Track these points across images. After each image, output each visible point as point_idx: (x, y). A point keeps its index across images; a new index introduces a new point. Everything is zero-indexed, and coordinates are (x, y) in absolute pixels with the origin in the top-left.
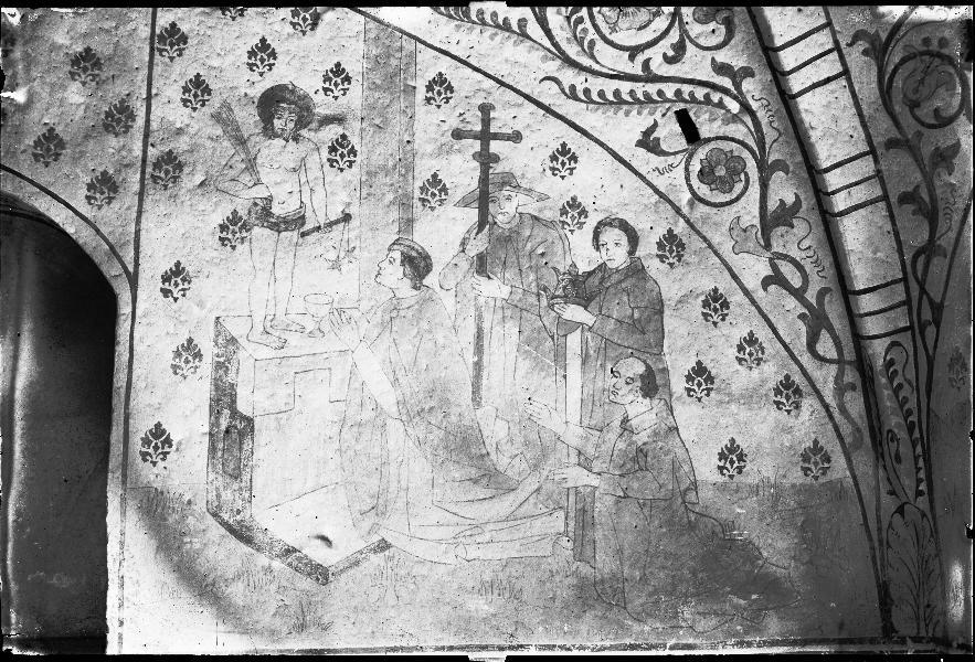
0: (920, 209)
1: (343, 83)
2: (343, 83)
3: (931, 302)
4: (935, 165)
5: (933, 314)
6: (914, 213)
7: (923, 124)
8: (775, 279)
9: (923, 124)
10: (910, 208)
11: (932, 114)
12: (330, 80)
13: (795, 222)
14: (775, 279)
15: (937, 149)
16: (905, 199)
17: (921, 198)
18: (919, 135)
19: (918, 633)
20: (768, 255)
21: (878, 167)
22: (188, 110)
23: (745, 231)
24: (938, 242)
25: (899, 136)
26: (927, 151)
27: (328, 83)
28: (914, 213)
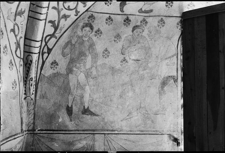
0: (54, 26)
1: (171, 3)
2: (171, 3)
3: (48, 48)
4: (62, 18)
5: (47, 51)
6: (51, 26)
7: (64, 7)
8: (13, 30)
9: (64, 7)
10: (51, 24)
11: (68, 6)
12: (97, 32)
13: (22, 16)
14: (13, 30)
15: (65, 14)
16: (50, 22)
17: (55, 23)
18: (62, 9)
19: (36, 150)
20: (14, 23)
21: (48, 12)
22: (168, 8)
23: (11, 13)
24: (55, 35)
25: (57, 8)
26: (62, 13)
27: (125, 22)
28: (51, 26)
